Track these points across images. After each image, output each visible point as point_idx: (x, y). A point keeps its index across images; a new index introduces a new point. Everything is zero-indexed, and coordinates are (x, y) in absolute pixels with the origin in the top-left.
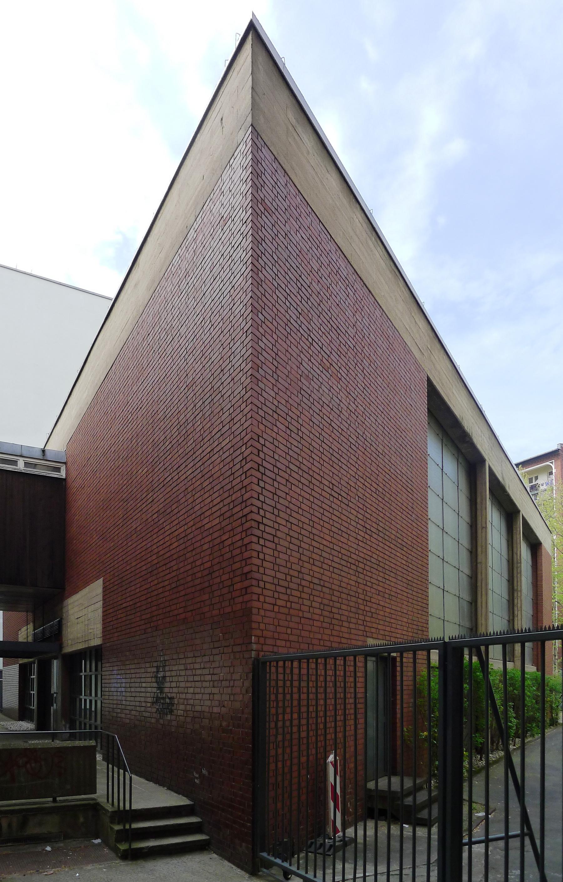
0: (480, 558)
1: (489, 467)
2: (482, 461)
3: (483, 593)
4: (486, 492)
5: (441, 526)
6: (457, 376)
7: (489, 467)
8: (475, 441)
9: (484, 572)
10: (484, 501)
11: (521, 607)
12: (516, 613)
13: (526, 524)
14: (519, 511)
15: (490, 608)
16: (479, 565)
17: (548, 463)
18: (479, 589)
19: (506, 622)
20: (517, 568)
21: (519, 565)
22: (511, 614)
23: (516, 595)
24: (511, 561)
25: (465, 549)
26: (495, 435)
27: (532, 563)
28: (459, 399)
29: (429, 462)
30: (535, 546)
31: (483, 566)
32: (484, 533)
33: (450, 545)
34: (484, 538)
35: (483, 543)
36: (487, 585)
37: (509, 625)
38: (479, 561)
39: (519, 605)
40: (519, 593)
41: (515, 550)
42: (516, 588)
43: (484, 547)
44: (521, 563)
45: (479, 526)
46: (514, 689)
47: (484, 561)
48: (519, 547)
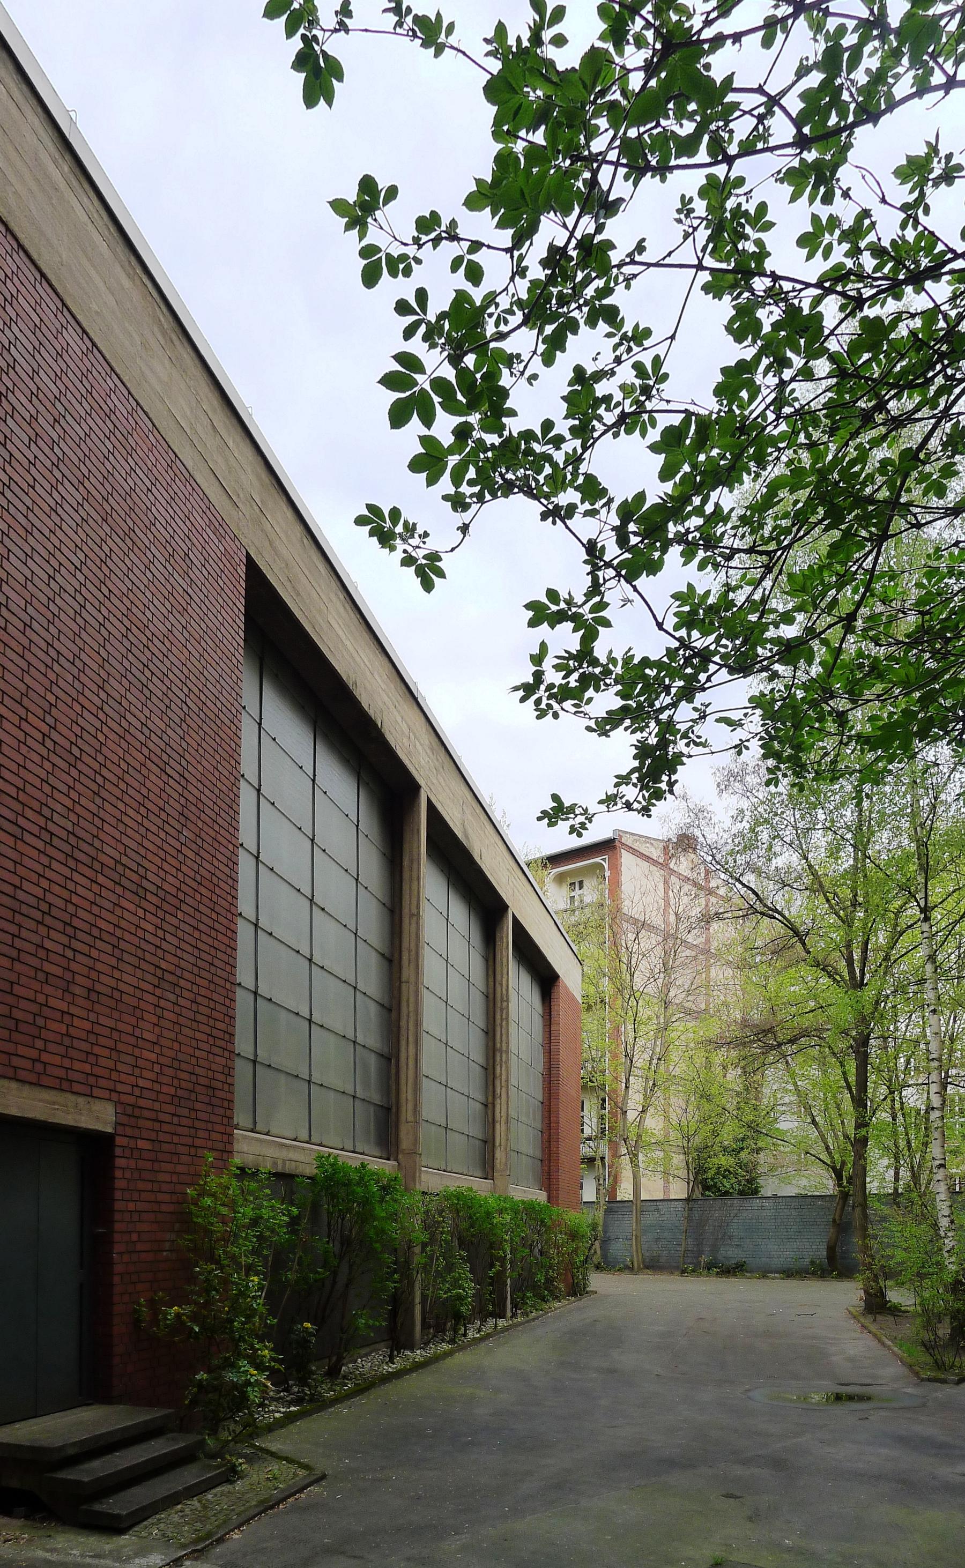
0: (407, 972)
1: (429, 801)
2: (414, 788)
3: (411, 1039)
4: (419, 847)
5: (307, 890)
6: (362, 628)
7: (429, 801)
8: (389, 737)
9: (412, 1000)
10: (415, 866)
11: (507, 1081)
12: (498, 1091)
13: (519, 929)
14: (506, 907)
15: (425, 1069)
16: (404, 986)
17: (598, 860)
18: (403, 1032)
19: (478, 1106)
20: (502, 1010)
21: (505, 1004)
22: (491, 1093)
23: (498, 1059)
24: (491, 996)
25: (374, 953)
26: (415, 699)
27: (544, 1010)
28: (348, 643)
29: (424, 905)
30: (546, 979)
31: (412, 988)
32: (414, 926)
33: (456, 1022)
34: (413, 936)
35: (413, 945)
36: (418, 1024)
37: (486, 1113)
38: (404, 978)
39: (504, 1077)
40: (504, 1056)
41: (498, 977)
42: (498, 1045)
43: (413, 953)
44: (508, 1001)
45: (406, 911)
46: (201, 1195)
47: (412, 979)
48: (505, 972)
